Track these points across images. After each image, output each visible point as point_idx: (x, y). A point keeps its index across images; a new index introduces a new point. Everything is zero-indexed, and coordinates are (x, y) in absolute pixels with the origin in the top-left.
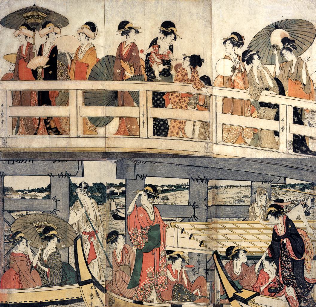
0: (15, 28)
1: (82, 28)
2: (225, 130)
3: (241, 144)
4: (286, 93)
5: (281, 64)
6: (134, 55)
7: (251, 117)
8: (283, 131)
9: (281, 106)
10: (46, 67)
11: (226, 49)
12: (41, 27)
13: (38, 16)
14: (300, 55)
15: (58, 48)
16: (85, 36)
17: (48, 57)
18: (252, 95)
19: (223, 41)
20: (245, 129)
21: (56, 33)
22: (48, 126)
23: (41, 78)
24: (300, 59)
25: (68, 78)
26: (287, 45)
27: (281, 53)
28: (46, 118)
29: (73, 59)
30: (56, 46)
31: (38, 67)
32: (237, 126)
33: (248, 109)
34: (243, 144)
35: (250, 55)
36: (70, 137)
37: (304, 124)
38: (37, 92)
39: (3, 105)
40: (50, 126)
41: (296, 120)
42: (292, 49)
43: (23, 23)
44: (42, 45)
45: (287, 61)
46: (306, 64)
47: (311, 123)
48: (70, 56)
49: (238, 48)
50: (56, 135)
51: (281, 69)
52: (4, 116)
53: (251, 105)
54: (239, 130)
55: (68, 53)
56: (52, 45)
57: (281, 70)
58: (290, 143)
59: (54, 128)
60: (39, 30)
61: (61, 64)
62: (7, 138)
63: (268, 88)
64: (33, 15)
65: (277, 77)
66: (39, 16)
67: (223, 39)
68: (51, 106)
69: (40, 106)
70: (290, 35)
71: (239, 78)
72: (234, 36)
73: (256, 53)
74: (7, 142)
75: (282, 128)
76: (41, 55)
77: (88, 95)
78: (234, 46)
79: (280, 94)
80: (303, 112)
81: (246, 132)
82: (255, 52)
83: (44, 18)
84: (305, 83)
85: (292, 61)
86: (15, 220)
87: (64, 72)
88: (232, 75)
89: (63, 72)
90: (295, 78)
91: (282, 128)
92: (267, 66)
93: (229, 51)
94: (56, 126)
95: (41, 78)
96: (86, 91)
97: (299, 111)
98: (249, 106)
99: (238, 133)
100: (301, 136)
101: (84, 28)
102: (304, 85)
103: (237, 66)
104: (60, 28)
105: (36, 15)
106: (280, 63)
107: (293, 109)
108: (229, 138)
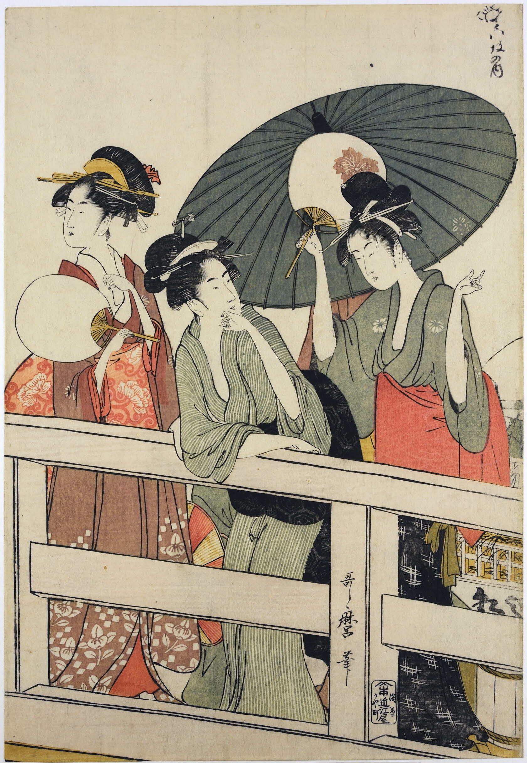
2: (61, 629)
3: (137, 696)
4: (366, 446)
5: (343, 303)
7: (191, 563)
8: (348, 633)
9: (337, 511)
11: (67, 231)
14: (437, 260)
18: (194, 456)
19: (55, 187)
20: (158, 623)
24: (435, 279)
26: (372, 211)
27: (343, 245)
32: (119, 609)
33: (174, 526)
34: (151, 696)
35: (180, 263)
37: (454, 598)
41: (414, 583)
42: (397, 229)
45: (372, 290)
46: (463, 302)
47: (490, 593)
49: (126, 225)
51: (340, 330)
53: (191, 507)
54: (128, 628)
57: (342, 339)
58: (384, 692)
63: (275, 422)
65: (321, 368)
67: (55, 178)
70: (392, 163)
71: (130, 374)
72: (105, 165)
73: (217, 248)
75: (347, 618)
77: (62, 272)
78: (106, 214)
79: (335, 452)
80: (449, 544)
81: (166, 640)
82: (211, 245)
84: (459, 399)
85: (395, 289)
88: (96, 357)
90: (411, 376)
91: (347, 618)
92: (268, 313)
93: (78, 241)
97: (431, 537)
98: (180, 512)
99: (122, 639)
100: (439, 659)
102: (454, 405)
103: (123, 315)
106: (334, 300)
107: (401, 525)
108: (77, 664)
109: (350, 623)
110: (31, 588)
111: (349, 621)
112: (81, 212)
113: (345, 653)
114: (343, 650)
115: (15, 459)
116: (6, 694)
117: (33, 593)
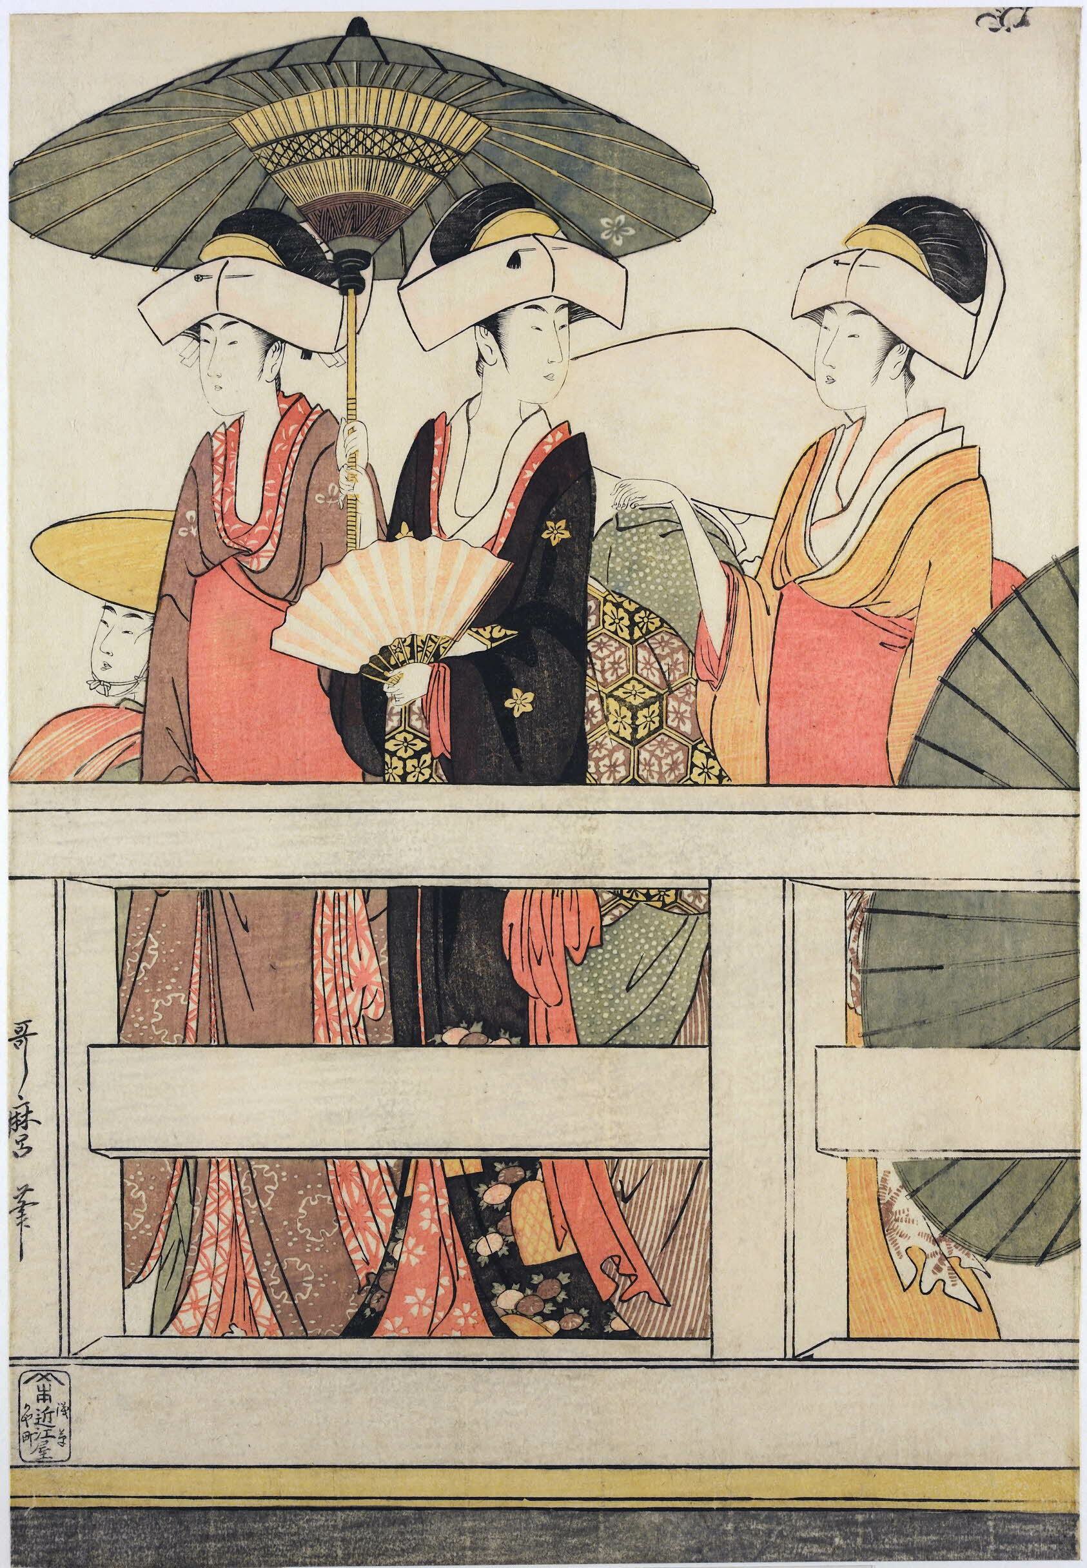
0: (157, 251)
1: (850, 258)
6: (421, 1288)
10: (470, 645)
12: (425, 254)
13: (393, 131)
15: (596, 457)
16: (878, 340)
17: (489, 546)
21: (576, 312)
22: (489, 1245)
23: (427, 757)
25: (699, 759)
28: (474, 1167)
29: (750, 569)
30: (582, 437)
31: (385, 650)
36: (711, 1362)
38: (379, 901)
39: (21, 1035)
40: (513, 1248)
43: (233, 206)
44: (439, 426)
48: (717, 537)
50: (574, 1334)
52: (42, 1137)
55: (698, 512)
56: (537, 429)
59: (549, 1269)
60: (402, 273)
61: (633, 625)
62: (73, 1368)
64: (346, 128)
66: (408, 134)
68: (525, 1044)
69: (414, 1042)
74: (67, 1410)
76: (422, 531)
83: (457, 153)
86: (755, 579)
87: (659, 697)
89: (647, 704)
94: (568, 1250)
95: (417, 755)
96: (878, 891)
101: (868, 258)
104: (614, 259)
105: (376, 128)
109: (26, 1128)
110: (90, 1146)
111: (24, 1125)
112: (853, 336)
113: (19, 1190)
114: (29, 1182)
115: (60, 882)
116: (1075, 1365)
117: (92, 1151)
